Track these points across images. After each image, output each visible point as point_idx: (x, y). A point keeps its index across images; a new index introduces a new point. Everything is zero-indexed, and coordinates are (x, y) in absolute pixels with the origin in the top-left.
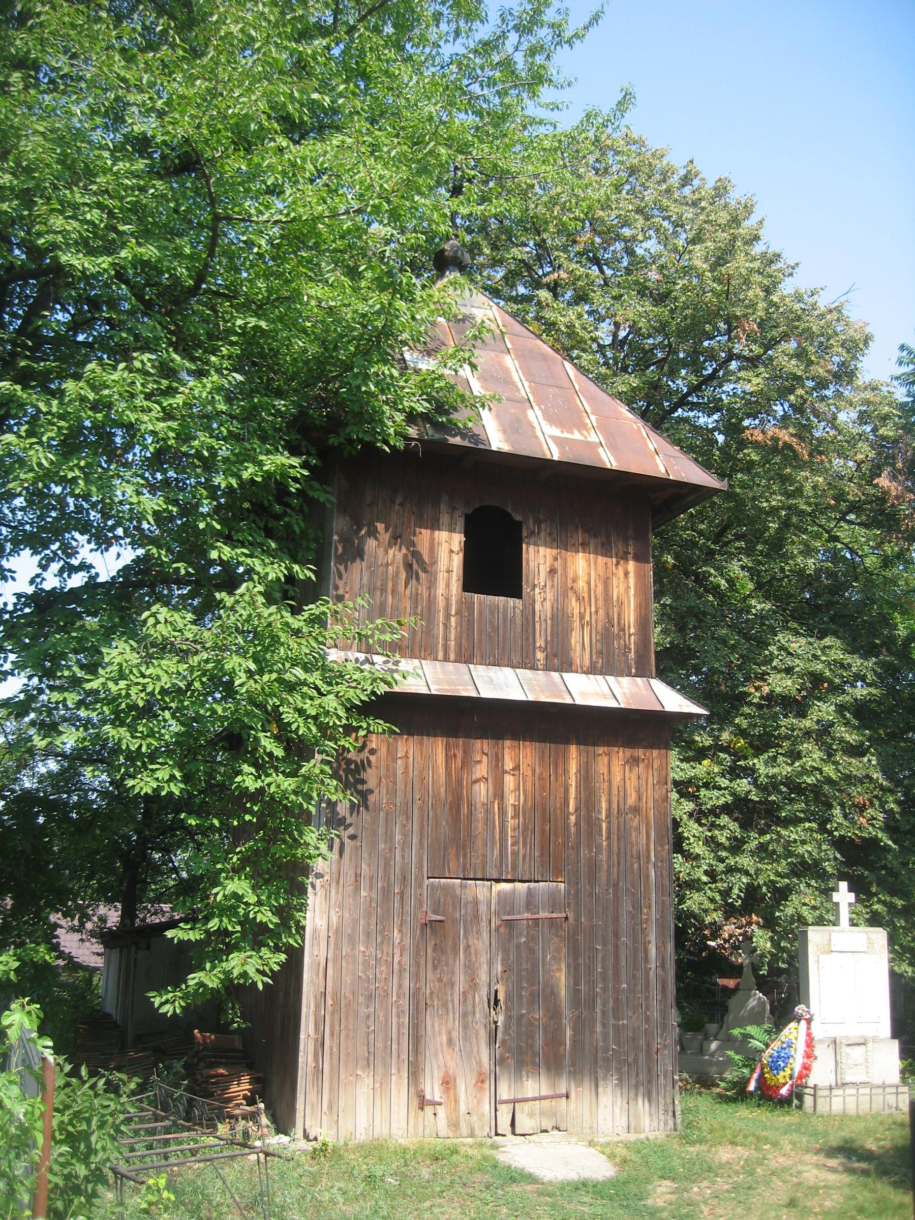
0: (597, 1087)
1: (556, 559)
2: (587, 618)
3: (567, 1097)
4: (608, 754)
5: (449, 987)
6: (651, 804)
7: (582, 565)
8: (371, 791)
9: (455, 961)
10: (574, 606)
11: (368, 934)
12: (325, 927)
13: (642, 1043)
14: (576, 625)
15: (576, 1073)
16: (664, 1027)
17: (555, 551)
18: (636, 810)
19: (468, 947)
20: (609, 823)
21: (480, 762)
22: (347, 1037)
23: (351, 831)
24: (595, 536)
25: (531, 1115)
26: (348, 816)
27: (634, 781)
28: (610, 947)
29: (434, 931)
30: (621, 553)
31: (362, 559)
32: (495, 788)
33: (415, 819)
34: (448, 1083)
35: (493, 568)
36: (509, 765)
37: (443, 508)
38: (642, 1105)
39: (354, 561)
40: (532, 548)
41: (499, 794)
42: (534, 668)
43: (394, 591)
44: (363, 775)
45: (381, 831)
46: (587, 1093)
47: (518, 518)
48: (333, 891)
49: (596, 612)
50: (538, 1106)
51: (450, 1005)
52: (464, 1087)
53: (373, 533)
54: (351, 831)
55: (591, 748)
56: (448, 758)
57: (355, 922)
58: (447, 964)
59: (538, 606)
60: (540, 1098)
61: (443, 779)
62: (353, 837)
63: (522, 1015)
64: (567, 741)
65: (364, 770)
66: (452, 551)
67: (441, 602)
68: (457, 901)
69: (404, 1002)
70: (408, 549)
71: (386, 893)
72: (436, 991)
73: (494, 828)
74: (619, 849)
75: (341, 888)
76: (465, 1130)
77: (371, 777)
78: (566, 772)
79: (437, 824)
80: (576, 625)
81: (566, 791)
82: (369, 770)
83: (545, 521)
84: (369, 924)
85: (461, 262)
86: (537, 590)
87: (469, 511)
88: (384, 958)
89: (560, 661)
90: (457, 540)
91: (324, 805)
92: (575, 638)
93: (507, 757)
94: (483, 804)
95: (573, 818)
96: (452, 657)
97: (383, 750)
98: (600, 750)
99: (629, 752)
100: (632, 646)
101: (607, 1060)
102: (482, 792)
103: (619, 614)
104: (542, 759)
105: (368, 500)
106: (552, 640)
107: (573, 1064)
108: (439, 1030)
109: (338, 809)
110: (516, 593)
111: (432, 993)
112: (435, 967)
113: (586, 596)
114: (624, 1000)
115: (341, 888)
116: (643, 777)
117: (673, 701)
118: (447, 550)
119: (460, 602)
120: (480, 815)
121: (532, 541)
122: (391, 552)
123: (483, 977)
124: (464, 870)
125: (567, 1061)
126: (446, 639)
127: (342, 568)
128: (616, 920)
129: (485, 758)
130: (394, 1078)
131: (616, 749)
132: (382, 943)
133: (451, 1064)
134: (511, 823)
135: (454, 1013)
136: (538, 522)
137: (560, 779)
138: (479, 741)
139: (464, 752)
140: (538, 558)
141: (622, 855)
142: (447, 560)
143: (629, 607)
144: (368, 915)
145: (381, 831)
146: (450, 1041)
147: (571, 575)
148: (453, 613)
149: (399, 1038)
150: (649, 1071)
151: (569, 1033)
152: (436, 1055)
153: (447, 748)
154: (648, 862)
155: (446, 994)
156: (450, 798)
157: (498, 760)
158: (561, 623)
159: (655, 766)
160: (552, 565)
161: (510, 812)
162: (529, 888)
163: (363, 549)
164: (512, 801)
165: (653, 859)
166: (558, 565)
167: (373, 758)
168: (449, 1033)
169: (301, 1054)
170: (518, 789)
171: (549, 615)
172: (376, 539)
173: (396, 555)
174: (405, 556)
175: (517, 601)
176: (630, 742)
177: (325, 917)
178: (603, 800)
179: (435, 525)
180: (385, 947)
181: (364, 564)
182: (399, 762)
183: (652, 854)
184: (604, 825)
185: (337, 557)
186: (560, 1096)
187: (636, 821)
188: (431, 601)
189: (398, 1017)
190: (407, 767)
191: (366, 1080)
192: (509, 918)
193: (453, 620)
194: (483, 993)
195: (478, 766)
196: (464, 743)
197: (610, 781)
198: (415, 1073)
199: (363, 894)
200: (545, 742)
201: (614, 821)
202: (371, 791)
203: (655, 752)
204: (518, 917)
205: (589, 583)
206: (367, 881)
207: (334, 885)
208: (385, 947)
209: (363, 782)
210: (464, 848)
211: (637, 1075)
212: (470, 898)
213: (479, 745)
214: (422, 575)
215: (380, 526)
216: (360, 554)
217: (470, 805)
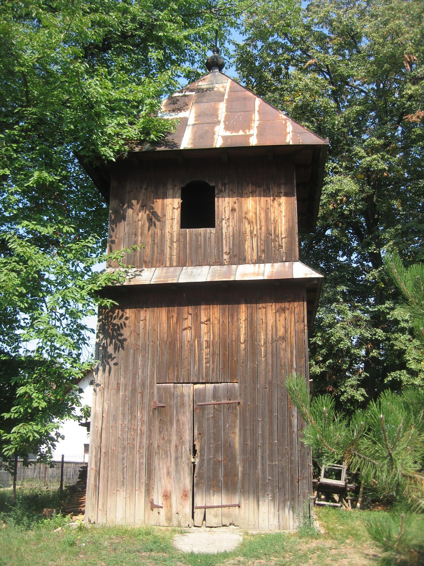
0: (258, 501)
1: (235, 203)
2: (255, 233)
3: (239, 507)
4: (265, 308)
5: (168, 443)
6: (293, 334)
7: (251, 204)
8: (125, 340)
9: (171, 428)
10: (248, 227)
11: (124, 415)
12: (101, 411)
13: (288, 475)
14: (248, 237)
15: (244, 492)
16: (303, 466)
17: (235, 199)
18: (283, 338)
19: (178, 420)
20: (266, 347)
21: (187, 319)
22: (112, 470)
23: (115, 361)
24: (259, 187)
25: (216, 516)
26: (113, 353)
27: (282, 322)
28: (267, 419)
29: (159, 412)
30: (276, 193)
31: (125, 220)
32: (196, 333)
33: (150, 352)
34: (167, 496)
35: (198, 213)
36: (204, 318)
37: (169, 186)
38: (288, 514)
39: (120, 222)
40: (220, 199)
41: (198, 335)
42: (222, 264)
43: (142, 234)
44: (122, 331)
45: (131, 360)
46: (251, 504)
47: (212, 184)
48: (106, 393)
49: (260, 229)
50: (220, 511)
51: (169, 453)
52: (175, 499)
53: (130, 206)
54: (115, 361)
55: (254, 305)
56: (168, 318)
57: (117, 408)
58: (167, 430)
59: (224, 231)
60: (222, 507)
61: (165, 330)
62: (116, 364)
63: (210, 459)
64: (239, 303)
65: (122, 328)
66: (174, 208)
67: (168, 236)
68: (172, 395)
69: (144, 451)
70: (149, 211)
71: (134, 391)
72: (161, 445)
73: (195, 354)
74: (272, 361)
75: (110, 391)
76: (175, 523)
77: (126, 332)
78: (238, 319)
79: (163, 354)
80: (248, 237)
81: (239, 330)
82: (124, 328)
83: (229, 183)
84: (124, 410)
85: (217, 64)
86: (224, 222)
87: (183, 186)
88: (132, 427)
89: (239, 258)
90: (177, 202)
91: (101, 348)
92: (247, 244)
93: (203, 315)
94: (189, 342)
95: (243, 346)
96: (175, 264)
97: (133, 316)
98: (260, 305)
99: (278, 305)
100: (284, 245)
101: (264, 485)
102: (188, 335)
103: (275, 228)
104: (224, 314)
105: (128, 190)
106: (233, 248)
107: (243, 487)
108: (162, 467)
109: (108, 350)
110: (212, 224)
111: (158, 446)
112: (160, 432)
113: (254, 220)
114: (276, 451)
115: (110, 391)
116: (288, 319)
117: (301, 271)
118: (171, 208)
119: (179, 234)
120: (186, 348)
121: (221, 195)
122: (140, 214)
123: (187, 437)
124: (177, 379)
125: (239, 485)
126: (171, 255)
127: (114, 226)
128: (270, 403)
129: (190, 317)
130: (137, 492)
131: (271, 304)
132: (131, 419)
133: (169, 486)
134: (205, 351)
135: (171, 457)
136: (224, 184)
137: (235, 324)
138: (186, 307)
139: (178, 314)
140: (224, 205)
141: (275, 365)
142: (171, 213)
143: (281, 223)
144: (124, 405)
145: (131, 360)
146: (168, 473)
147: (245, 210)
148: (175, 240)
149: (140, 470)
150: (293, 492)
151: (240, 469)
152: (160, 480)
153: (168, 312)
154: (292, 368)
155: (166, 447)
156: (170, 339)
157: (197, 316)
158: (239, 238)
159: (296, 312)
160: (233, 207)
161: (204, 345)
162: (215, 387)
163: (125, 215)
164: (206, 339)
165: (295, 366)
166: (236, 206)
167: (127, 322)
168: (168, 468)
169: (88, 478)
170: (209, 332)
171: (231, 234)
172: (132, 209)
173: (143, 215)
174: (148, 215)
175: (212, 229)
176: (278, 300)
177: (101, 406)
178: (262, 334)
179: (164, 196)
180: (133, 422)
181: (126, 223)
182: (141, 322)
183: (295, 363)
184: (263, 349)
185: (111, 221)
186: (235, 506)
187: (284, 344)
188: (163, 236)
189: (140, 459)
190: (145, 325)
191: (122, 493)
192: (202, 404)
193: (175, 245)
194: (187, 446)
195: (186, 321)
196: (177, 310)
197: (266, 323)
198: (148, 491)
199: (121, 393)
200: (226, 304)
201: (269, 345)
202: (125, 340)
203: (296, 304)
204: (208, 403)
205: (256, 214)
206: (124, 387)
207: (106, 389)
208: (133, 422)
209: (121, 335)
210: (177, 365)
211: (285, 495)
212: (179, 393)
213: (186, 310)
214: (158, 223)
215: (134, 202)
216: (124, 218)
217: (181, 342)
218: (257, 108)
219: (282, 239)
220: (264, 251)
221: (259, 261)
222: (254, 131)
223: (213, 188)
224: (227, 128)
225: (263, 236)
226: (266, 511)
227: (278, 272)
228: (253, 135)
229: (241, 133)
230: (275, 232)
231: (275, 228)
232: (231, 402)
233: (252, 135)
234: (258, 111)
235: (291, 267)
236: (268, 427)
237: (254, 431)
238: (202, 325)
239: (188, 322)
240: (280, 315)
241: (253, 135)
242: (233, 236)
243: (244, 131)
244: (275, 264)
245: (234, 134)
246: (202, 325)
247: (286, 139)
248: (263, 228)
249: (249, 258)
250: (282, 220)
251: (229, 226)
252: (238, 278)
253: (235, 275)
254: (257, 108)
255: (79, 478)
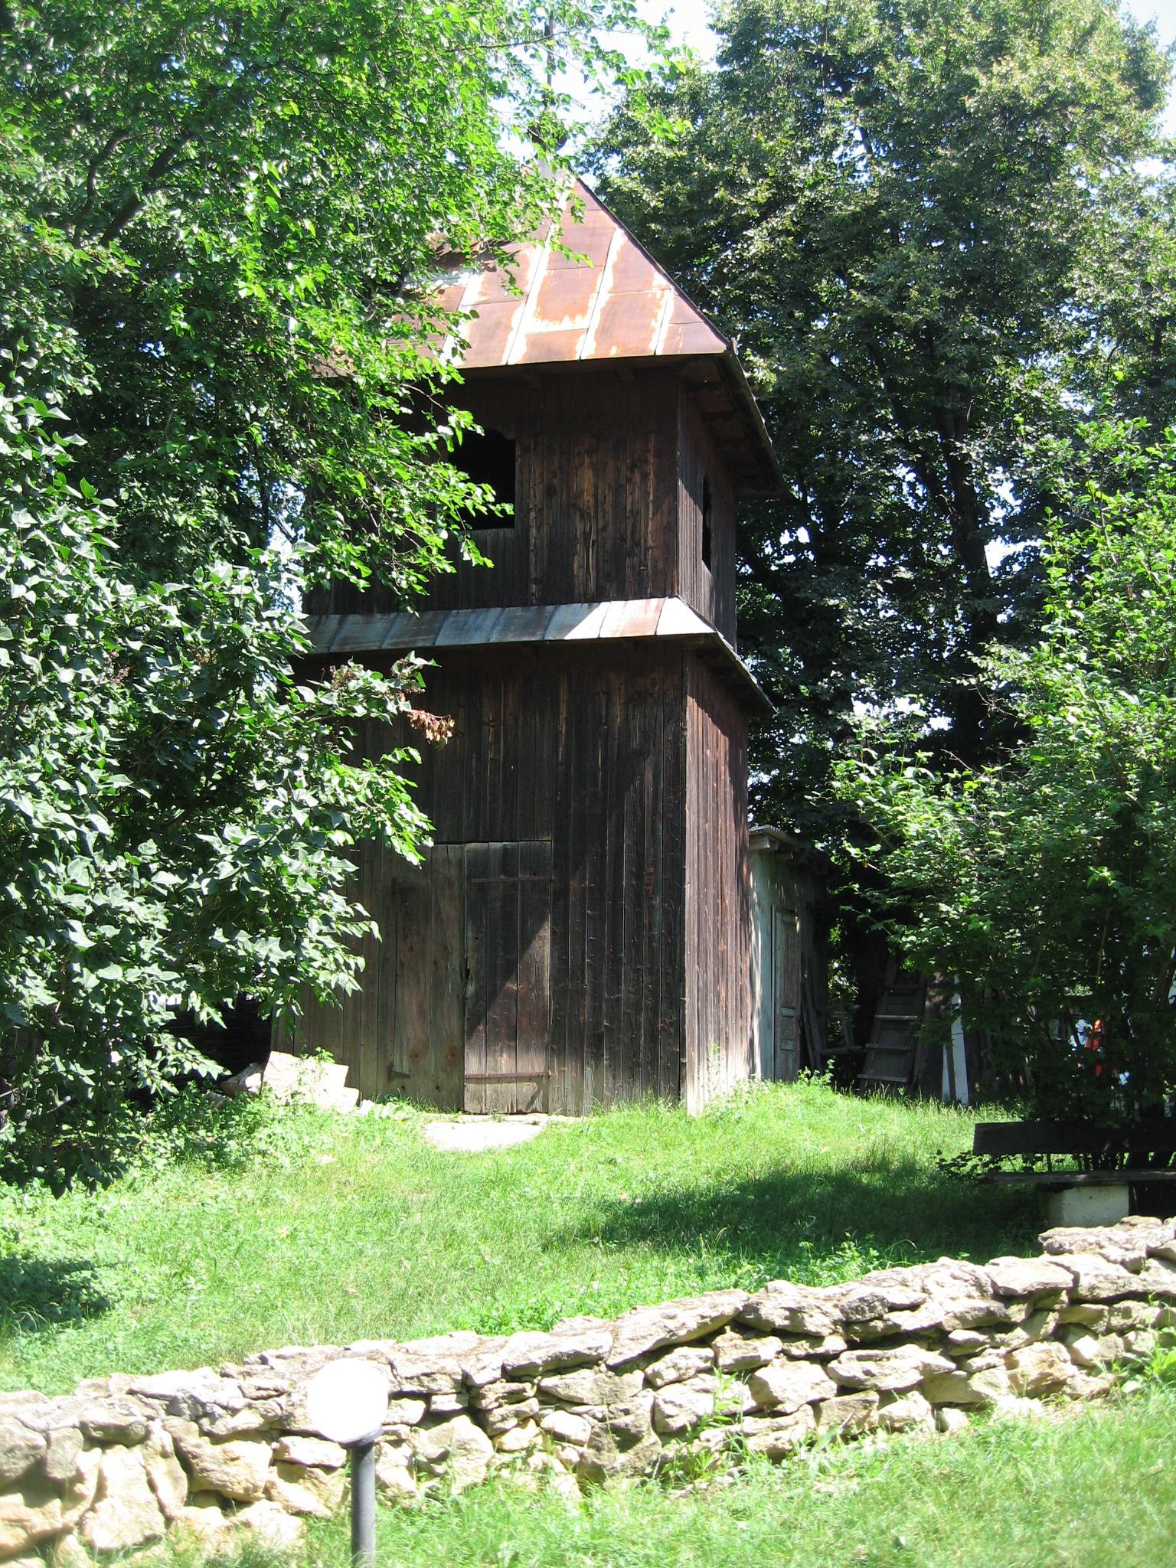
19: (439, 914)
47: (510, 436)
86: (533, 515)
112: (405, 937)
218: (613, 258)
222: (592, 320)
223: (511, 444)
224: (544, 314)
230: (633, 533)
234: (615, 267)
249: (579, 589)
254: (613, 258)
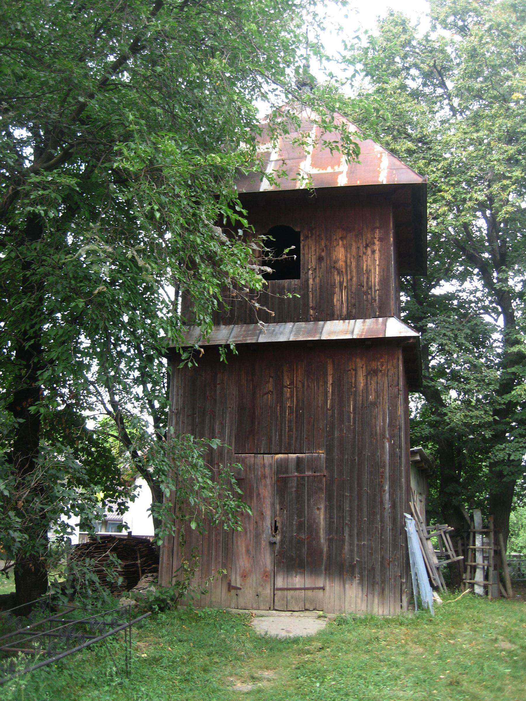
2: (345, 284)
19: (259, 494)
47: (297, 230)
49: (351, 279)
59: (311, 281)
60: (305, 589)
80: (337, 290)
86: (310, 272)
93: (286, 378)
103: (368, 278)
129: (271, 380)
140: (310, 255)
146: (248, 551)
160: (320, 255)
186: (320, 588)
211: (374, 578)
219: (375, 291)
220: (355, 305)
221: (349, 316)
223: (299, 233)
225: (354, 287)
226: (353, 596)
227: (369, 330)
228: (342, 172)
229: (329, 170)
231: (368, 278)
232: (316, 474)
233: (341, 173)
235: (385, 324)
236: (356, 503)
237: (340, 508)
238: (285, 389)
239: (270, 386)
240: (371, 379)
241: (342, 172)
242: (320, 288)
243: (332, 168)
244: (367, 320)
245: (321, 171)
246: (285, 389)
247: (378, 177)
248: (354, 279)
249: (337, 313)
250: (375, 269)
251: (315, 277)
252: (324, 337)
253: (321, 333)
255: (238, 346)
